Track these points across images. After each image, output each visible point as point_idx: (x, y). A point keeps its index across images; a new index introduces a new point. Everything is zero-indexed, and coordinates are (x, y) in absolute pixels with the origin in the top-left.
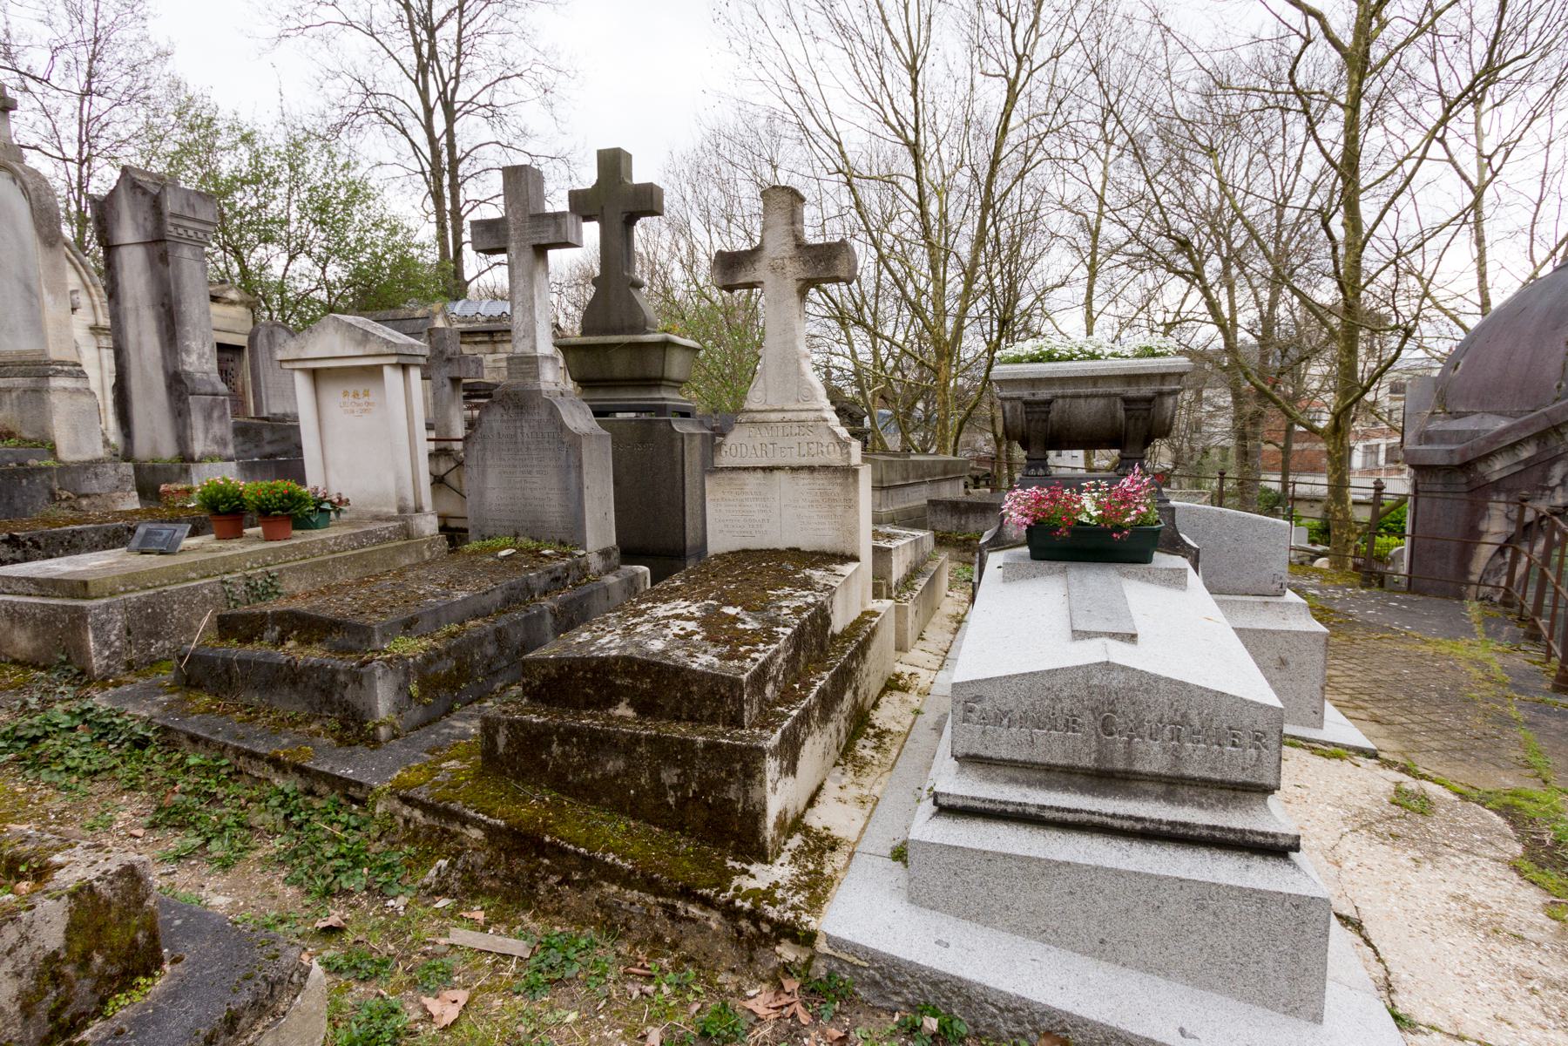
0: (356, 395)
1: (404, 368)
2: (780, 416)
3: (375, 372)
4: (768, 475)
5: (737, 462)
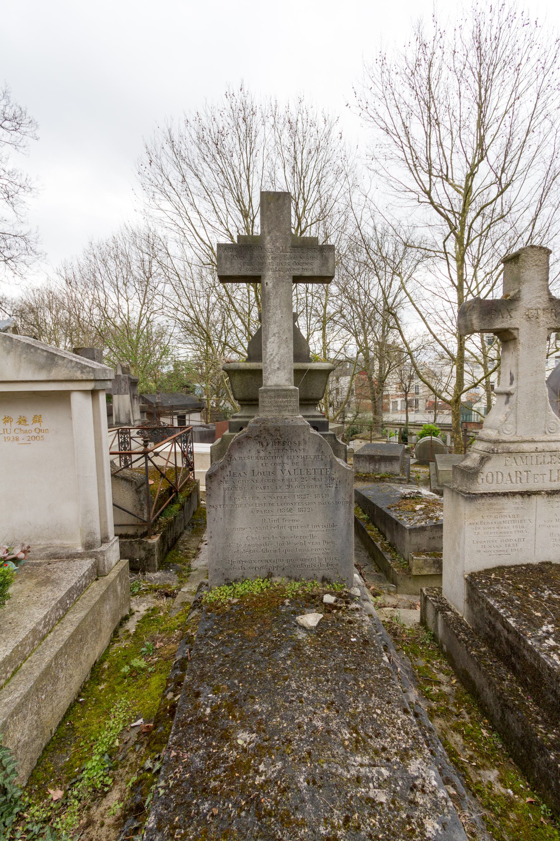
0: (23, 421)
1: (94, 393)
2: (532, 446)
3: (63, 397)
4: (526, 499)
5: (493, 488)
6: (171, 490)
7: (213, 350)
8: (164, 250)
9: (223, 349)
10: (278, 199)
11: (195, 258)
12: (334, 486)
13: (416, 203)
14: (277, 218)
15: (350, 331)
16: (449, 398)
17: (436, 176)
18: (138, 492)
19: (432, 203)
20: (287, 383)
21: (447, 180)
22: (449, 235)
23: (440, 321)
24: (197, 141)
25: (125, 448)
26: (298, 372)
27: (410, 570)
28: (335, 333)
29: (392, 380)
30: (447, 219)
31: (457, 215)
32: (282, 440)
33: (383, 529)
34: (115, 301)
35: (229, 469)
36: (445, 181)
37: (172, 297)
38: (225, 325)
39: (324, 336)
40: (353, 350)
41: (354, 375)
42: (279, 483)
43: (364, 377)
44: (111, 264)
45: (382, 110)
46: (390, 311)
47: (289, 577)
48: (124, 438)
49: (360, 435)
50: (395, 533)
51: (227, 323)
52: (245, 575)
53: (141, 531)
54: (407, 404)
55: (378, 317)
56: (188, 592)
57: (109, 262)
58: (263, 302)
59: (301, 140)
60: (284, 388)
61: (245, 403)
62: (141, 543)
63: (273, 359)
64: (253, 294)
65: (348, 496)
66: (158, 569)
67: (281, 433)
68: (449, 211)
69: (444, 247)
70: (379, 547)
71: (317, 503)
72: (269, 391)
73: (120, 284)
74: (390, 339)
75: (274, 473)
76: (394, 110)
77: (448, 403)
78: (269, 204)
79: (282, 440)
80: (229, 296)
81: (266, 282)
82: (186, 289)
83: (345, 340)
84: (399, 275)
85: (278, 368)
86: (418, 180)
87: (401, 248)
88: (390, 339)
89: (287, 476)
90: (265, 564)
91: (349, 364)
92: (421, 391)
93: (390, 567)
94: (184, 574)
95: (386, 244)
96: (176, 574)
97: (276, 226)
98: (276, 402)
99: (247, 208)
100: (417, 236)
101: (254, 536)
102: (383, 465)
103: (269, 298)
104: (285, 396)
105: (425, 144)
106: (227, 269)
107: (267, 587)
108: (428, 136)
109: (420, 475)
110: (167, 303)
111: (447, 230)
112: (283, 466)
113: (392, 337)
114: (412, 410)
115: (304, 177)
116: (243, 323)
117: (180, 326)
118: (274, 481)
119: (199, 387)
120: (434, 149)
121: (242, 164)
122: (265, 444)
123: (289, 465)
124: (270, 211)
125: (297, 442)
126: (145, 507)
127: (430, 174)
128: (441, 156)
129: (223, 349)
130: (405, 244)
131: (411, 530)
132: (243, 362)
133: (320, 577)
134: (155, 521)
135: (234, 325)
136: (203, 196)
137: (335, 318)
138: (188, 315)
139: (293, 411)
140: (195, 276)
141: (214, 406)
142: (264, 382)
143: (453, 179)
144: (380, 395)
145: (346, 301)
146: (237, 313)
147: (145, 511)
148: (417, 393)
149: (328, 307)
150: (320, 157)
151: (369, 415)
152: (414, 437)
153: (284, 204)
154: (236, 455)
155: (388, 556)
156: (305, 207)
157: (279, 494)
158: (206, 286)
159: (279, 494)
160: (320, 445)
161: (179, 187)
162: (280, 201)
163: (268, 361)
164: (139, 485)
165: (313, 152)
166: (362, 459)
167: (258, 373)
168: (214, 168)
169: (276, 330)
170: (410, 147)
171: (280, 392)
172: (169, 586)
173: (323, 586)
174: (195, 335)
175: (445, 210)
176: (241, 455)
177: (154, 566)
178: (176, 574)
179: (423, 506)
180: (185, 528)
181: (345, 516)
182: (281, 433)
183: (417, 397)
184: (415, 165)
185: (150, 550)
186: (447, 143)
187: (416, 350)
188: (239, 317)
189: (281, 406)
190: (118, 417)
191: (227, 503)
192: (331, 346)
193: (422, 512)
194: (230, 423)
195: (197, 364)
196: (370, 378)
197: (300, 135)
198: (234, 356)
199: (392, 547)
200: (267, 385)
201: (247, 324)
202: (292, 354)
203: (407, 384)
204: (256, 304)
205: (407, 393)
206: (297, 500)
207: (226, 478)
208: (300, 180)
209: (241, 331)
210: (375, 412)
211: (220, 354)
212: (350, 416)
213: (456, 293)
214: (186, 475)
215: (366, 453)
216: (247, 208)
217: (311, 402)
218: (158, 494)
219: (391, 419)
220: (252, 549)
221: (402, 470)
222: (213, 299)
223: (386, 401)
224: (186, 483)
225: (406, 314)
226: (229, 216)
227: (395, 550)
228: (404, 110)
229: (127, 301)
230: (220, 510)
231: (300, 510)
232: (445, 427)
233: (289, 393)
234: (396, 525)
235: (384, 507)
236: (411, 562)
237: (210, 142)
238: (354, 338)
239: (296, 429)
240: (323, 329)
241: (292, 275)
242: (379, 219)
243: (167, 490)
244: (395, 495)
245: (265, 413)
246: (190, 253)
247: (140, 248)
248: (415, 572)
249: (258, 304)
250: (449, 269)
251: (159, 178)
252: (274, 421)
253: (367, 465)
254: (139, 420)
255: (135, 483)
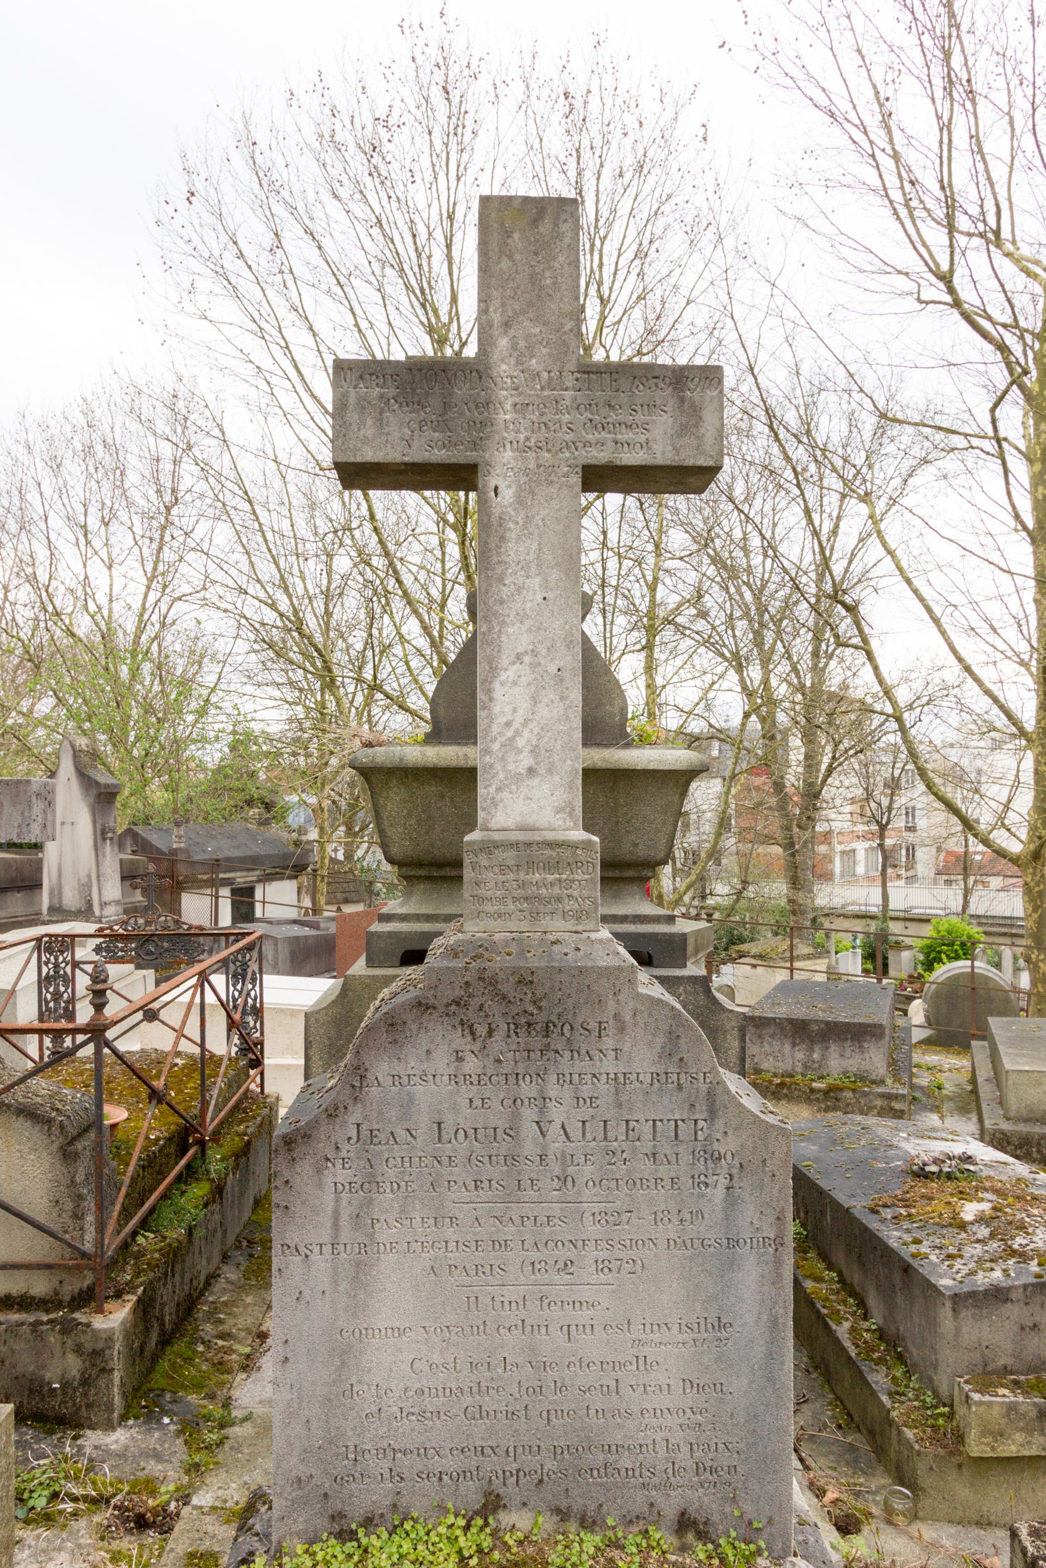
6: (185, 1137)
7: (338, 704)
8: (216, 432)
9: (369, 701)
10: (536, 221)
11: (299, 450)
12: (723, 1182)
13: (912, 304)
14: (534, 278)
15: (722, 655)
16: (1015, 847)
17: (970, 235)
18: (67, 1155)
19: (957, 304)
20: (558, 821)
21: (998, 242)
22: (1006, 392)
23: (984, 629)
24: (316, 145)
25: (57, 996)
26: (591, 776)
27: (960, 1438)
28: (679, 661)
29: (842, 791)
30: (1002, 348)
31: (1028, 338)
32: (540, 1018)
33: (856, 1277)
34: (78, 568)
35: (355, 1115)
36: (992, 248)
37: (233, 558)
38: (375, 632)
39: (650, 669)
40: (730, 708)
41: (733, 776)
42: (530, 1170)
43: (759, 781)
44: (74, 470)
45: (819, 61)
46: (837, 601)
47: (558, 1511)
48: (56, 966)
49: (753, 948)
50: (899, 1299)
51: (380, 630)
52: (403, 1502)
53: (72, 1286)
54: (885, 858)
55: (803, 611)
56: (214, 1508)
57: (67, 463)
58: (481, 566)
59: (598, 142)
60: (550, 836)
61: (421, 872)
62: (68, 1328)
63: (512, 739)
64: (453, 551)
65: (771, 1219)
66: (124, 1418)
67: (539, 992)
68: (1005, 326)
69: (994, 422)
70: (847, 1344)
71: (662, 1244)
72: (498, 845)
73: (93, 523)
74: (835, 676)
75: (512, 1132)
76: (850, 61)
77: (1015, 860)
78: (508, 234)
79: (540, 1018)
80: (387, 554)
81: (492, 484)
82: (269, 536)
83: (708, 679)
84: (866, 498)
85: (531, 771)
86: (918, 244)
87: (868, 422)
88: (835, 676)
89: (556, 1145)
90: (473, 1462)
91: (716, 744)
92: (921, 823)
93: (890, 1422)
94: (206, 1438)
95: (824, 421)
96: (180, 1433)
97: (531, 305)
98: (523, 885)
99: (445, 319)
100: (914, 395)
101: (436, 1358)
102: (834, 1049)
103: (502, 538)
104: (550, 866)
105: (937, 150)
106: (365, 441)
107: (480, 1551)
108: (946, 127)
109: (942, 1078)
110: (218, 575)
111: (1001, 377)
112: (542, 1110)
113: (848, 674)
114: (899, 876)
115: (603, 241)
116: (426, 629)
117: (252, 637)
118: (512, 1159)
119: (299, 806)
120: (962, 164)
121: (435, 202)
122: (481, 1030)
123: (561, 1107)
124: (510, 257)
125: (593, 1025)
126: (90, 1203)
127: (951, 228)
128: (982, 179)
129: (369, 701)
130: (883, 416)
131: (959, 1300)
132: (416, 742)
133: (671, 1512)
134: (125, 1246)
135: (399, 633)
136: (324, 287)
137: (679, 620)
138: (273, 606)
139: (579, 916)
140: (298, 500)
141: (340, 856)
142: (481, 815)
143: (1014, 242)
144: (808, 834)
145: (711, 571)
146: (409, 603)
147: (90, 1218)
148: (911, 829)
149: (660, 587)
150: (647, 189)
151: (778, 889)
152: (906, 955)
153: (559, 236)
154: (382, 1069)
155: (879, 1379)
156: (603, 318)
157: (527, 1209)
158: (323, 527)
159: (527, 1209)
160: (673, 1038)
161: (263, 263)
162: (545, 226)
163: (496, 746)
164: (72, 1131)
165: (628, 176)
166: (772, 1029)
167: (464, 778)
168: (358, 212)
169: (524, 643)
170: (896, 157)
171: (534, 852)
172: (150, 1486)
173: (683, 1548)
174: (292, 662)
175: (994, 323)
176: (400, 1069)
177: (110, 1408)
178: (180, 1433)
179: (986, 1206)
180: (225, 1258)
181: (760, 1289)
182: (539, 992)
183: (910, 837)
184: (907, 205)
185: (96, 1353)
186: (997, 144)
187: (911, 707)
188: (415, 612)
189: (538, 897)
190: (57, 892)
191: (345, 1236)
192: (668, 695)
193: (984, 1232)
194: (370, 935)
195: (296, 740)
196: (779, 787)
197: (594, 128)
198: (397, 722)
199: (891, 1344)
200: (493, 825)
201: (436, 633)
202: (577, 723)
203: (885, 802)
204: (462, 578)
205: (883, 828)
206: (592, 1229)
207: (345, 1147)
208: (592, 246)
209: (419, 652)
210: (795, 882)
211: (359, 715)
212: (721, 891)
213: (1030, 549)
214: (238, 1080)
215: (781, 1012)
216: (445, 319)
217: (630, 873)
218: (136, 1154)
219: (837, 902)
220: (431, 1404)
221: (893, 1064)
222: (343, 563)
223: (822, 849)
224: (236, 1107)
225: (887, 611)
226: (393, 339)
227: (900, 1358)
228: (879, 59)
229: (110, 568)
230: (321, 1262)
231: (602, 1266)
232: (1001, 929)
233: (567, 853)
234: (905, 1274)
235: (858, 1205)
236: (961, 1410)
237: (352, 148)
238: (732, 671)
239: (585, 977)
240: (648, 647)
241: (582, 462)
242: (807, 348)
243: (169, 1139)
244: (887, 1160)
245: (483, 922)
246: (284, 440)
247: (149, 425)
248: (976, 1447)
249: (469, 578)
250: (1007, 483)
251: (210, 236)
252: (514, 949)
253: (787, 1048)
254: (117, 903)
255: (62, 1126)
